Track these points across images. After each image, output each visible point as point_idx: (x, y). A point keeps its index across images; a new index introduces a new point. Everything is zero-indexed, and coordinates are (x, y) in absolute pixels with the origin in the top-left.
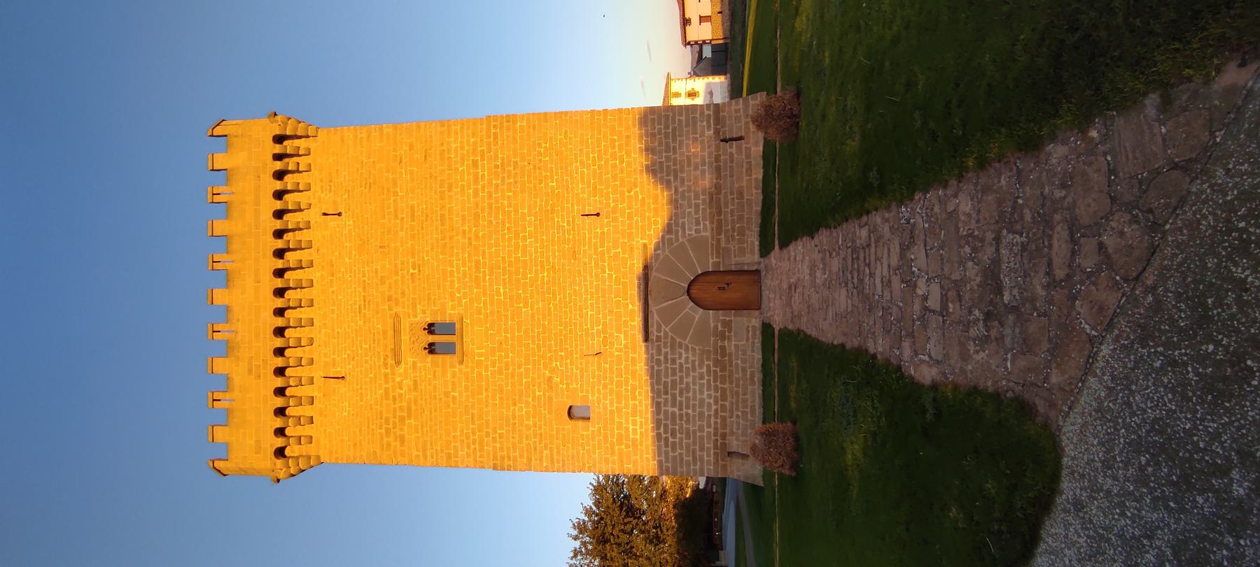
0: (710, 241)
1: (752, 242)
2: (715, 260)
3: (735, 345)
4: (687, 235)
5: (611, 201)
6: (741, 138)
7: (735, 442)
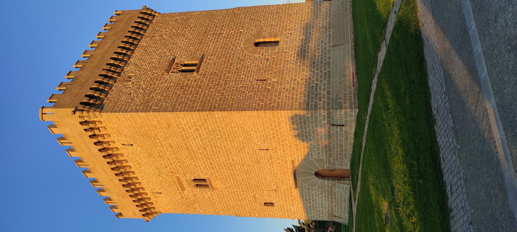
1: (347, 163)
2: (328, 166)
3: (301, 150)
6: (343, 126)
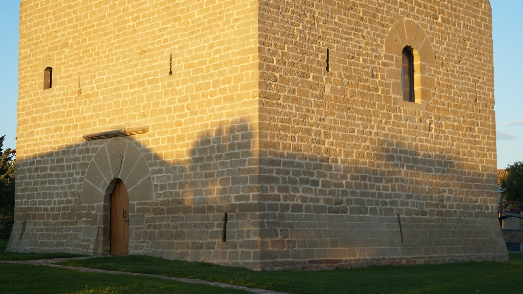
0: (149, 201)
2: (136, 207)
4: (154, 176)
5: (46, 200)
7: (30, 227)
